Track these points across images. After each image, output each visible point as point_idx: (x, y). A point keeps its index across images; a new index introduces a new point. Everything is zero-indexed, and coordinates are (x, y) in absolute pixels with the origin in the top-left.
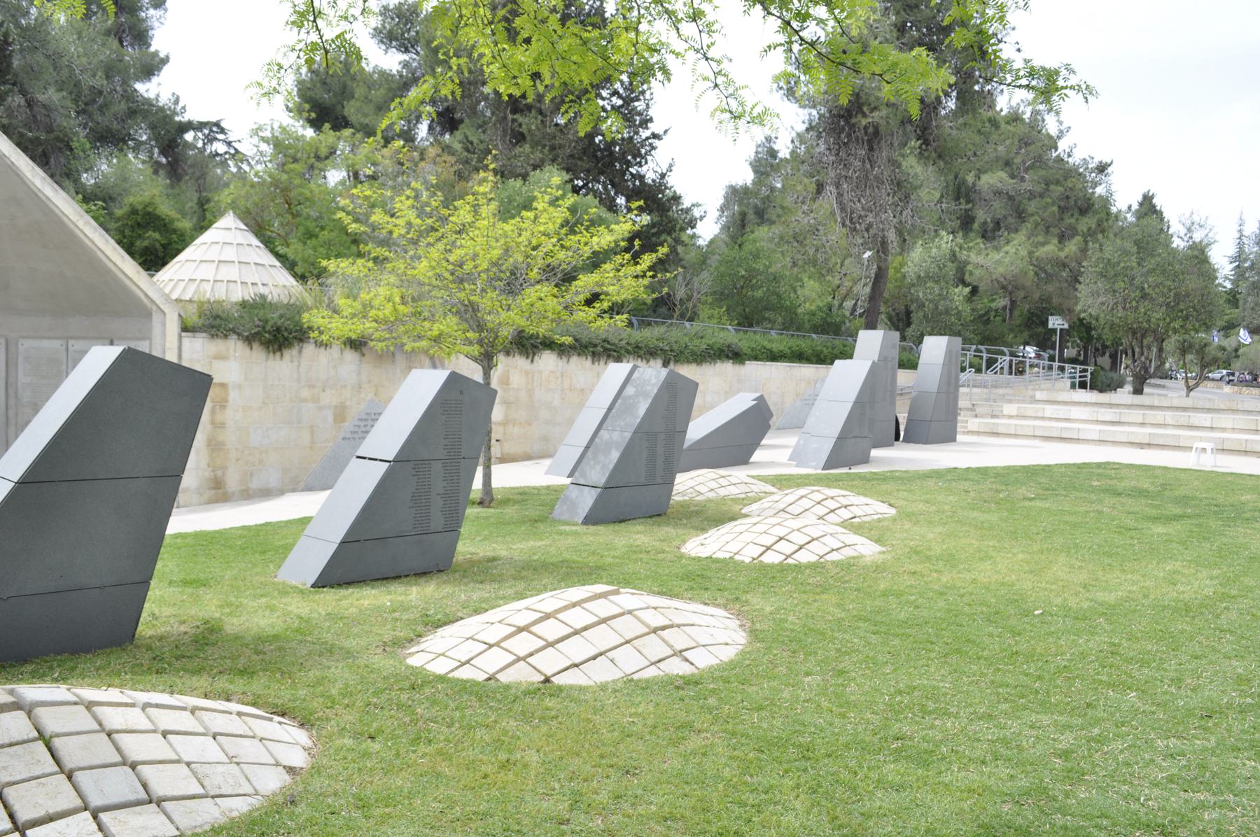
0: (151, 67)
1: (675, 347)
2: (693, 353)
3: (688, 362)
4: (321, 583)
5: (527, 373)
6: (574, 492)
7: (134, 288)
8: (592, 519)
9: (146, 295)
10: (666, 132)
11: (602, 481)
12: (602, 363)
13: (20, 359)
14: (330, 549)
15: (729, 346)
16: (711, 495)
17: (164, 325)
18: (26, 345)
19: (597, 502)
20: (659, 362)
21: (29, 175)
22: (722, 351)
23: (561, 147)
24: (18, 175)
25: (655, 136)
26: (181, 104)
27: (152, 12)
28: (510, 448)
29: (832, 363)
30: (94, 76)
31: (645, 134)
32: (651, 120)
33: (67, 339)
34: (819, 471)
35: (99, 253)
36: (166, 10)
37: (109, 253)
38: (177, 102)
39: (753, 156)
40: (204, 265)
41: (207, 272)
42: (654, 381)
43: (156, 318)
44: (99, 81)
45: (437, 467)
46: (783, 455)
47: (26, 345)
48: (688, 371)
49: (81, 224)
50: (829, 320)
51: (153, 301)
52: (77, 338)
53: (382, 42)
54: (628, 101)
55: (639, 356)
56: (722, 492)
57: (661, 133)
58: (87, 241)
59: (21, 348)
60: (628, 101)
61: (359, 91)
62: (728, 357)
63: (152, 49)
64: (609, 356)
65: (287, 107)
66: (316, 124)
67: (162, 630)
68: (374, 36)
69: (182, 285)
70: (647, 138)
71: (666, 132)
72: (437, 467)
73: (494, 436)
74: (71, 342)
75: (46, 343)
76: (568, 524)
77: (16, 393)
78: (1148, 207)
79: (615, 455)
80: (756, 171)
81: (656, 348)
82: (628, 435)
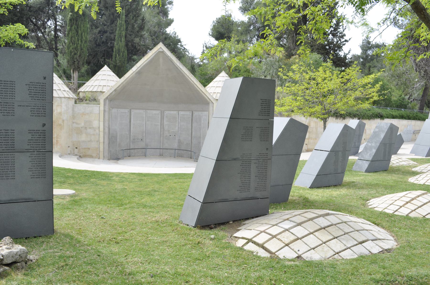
0: (169, 23)
1: (362, 114)
2: (368, 116)
3: (366, 119)
4: (311, 187)
5: (316, 122)
6: (360, 162)
7: (205, 96)
8: (368, 171)
9: (208, 98)
10: (350, 39)
11: (370, 159)
12: (339, 119)
13: (165, 117)
14: (314, 177)
15: (379, 114)
16: (397, 164)
17: (213, 107)
18: (166, 113)
19: (369, 165)
20: (357, 118)
21: (175, 62)
22: (377, 115)
23: (315, 46)
24: (172, 62)
25: (346, 41)
26: (177, 35)
27: (169, 6)
28: (310, 147)
29: (425, 120)
30: (154, 27)
31: (343, 40)
32: (345, 35)
33: (179, 111)
34: (424, 157)
35: (195, 85)
36: (173, 5)
37: (198, 85)
38: (175, 34)
39: (361, 44)
40: (217, 88)
41: (103, 83)
42: (385, 127)
43: (211, 105)
44: (156, 29)
45: (340, 153)
46: (408, 151)
47: (166, 113)
48: (365, 121)
49: (190, 76)
50: (402, 103)
51: (210, 100)
52: (181, 111)
53: (242, 11)
54: (335, 29)
55: (351, 117)
56: (401, 163)
57: (348, 40)
58: (191, 81)
59: (165, 114)
60: (335, 29)
61: (235, 28)
62: (379, 117)
63: (169, 18)
64: (341, 117)
65: (209, 34)
66: (217, 39)
67: (294, 198)
68: (240, 9)
69: (93, 87)
70: (343, 42)
71: (350, 39)
72: (340, 153)
73: (305, 143)
74: (180, 112)
75: (172, 112)
76: (359, 172)
77: (163, 127)
78: (171, 21)
79: (374, 151)
80: (362, 49)
81: (356, 114)
82: (378, 144)
